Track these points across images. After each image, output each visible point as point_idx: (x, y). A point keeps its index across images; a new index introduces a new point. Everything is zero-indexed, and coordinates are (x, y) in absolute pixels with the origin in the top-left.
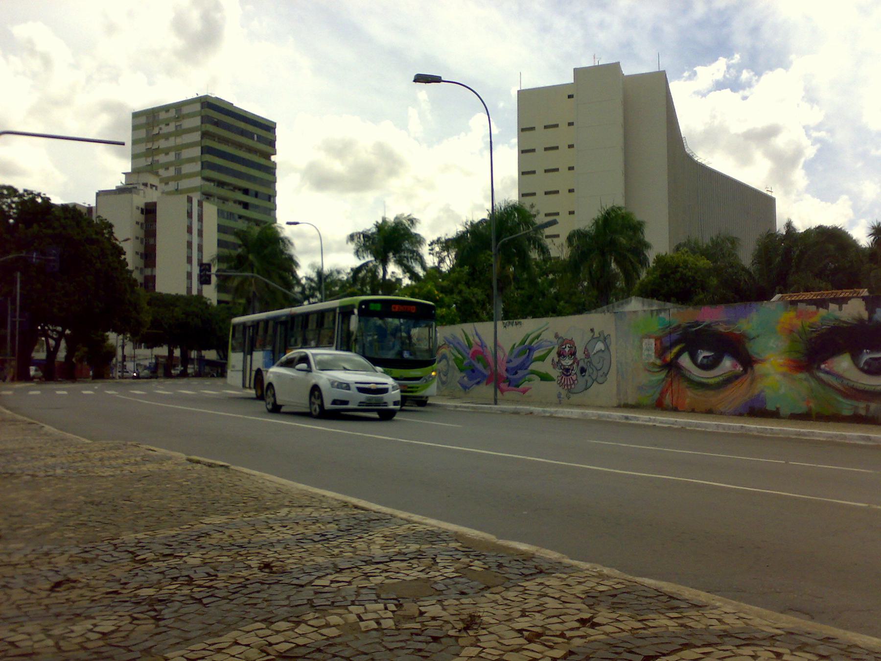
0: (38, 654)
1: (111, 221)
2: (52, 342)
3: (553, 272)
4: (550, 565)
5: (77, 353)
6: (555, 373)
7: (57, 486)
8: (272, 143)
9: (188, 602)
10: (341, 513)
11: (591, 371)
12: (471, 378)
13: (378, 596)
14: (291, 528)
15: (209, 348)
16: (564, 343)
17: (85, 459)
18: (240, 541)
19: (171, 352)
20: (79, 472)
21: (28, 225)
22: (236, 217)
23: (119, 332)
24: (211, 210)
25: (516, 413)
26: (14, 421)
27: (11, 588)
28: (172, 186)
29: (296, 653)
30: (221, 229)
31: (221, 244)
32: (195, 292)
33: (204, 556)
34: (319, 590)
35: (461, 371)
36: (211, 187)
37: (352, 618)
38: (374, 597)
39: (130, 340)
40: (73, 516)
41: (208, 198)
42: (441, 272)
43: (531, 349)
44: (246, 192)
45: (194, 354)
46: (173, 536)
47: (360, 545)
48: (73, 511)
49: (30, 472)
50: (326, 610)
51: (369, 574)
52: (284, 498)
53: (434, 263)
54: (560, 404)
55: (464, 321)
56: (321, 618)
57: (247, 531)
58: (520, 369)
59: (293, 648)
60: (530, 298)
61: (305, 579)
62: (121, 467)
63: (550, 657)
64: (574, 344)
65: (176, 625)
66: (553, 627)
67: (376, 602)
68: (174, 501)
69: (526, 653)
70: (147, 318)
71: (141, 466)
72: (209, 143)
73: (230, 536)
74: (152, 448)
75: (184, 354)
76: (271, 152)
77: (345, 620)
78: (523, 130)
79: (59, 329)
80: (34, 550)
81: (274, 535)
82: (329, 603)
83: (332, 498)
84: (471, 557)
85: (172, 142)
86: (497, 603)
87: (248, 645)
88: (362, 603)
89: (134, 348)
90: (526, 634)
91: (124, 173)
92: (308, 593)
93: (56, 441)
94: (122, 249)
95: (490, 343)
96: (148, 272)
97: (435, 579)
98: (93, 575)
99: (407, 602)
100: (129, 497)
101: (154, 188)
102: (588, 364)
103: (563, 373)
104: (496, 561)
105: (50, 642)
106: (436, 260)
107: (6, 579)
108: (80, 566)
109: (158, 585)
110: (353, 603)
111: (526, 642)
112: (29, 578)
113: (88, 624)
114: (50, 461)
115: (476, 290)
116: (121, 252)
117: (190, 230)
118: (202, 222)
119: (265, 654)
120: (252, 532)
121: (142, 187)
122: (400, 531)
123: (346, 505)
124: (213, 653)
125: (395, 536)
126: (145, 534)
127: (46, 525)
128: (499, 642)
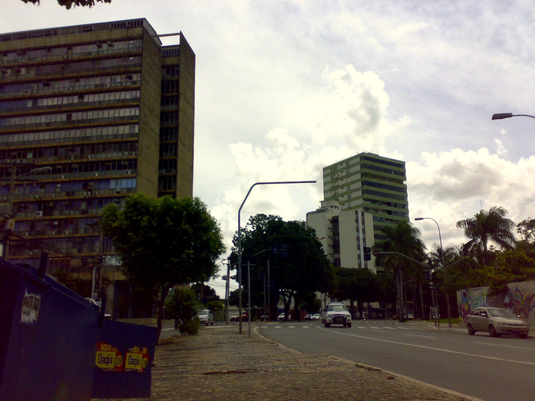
1: (314, 228)
2: (287, 298)
5: (301, 305)
7: (278, 378)
8: (403, 174)
19: (352, 304)
20: (291, 370)
22: (384, 220)
24: (369, 217)
26: (264, 342)
28: (346, 206)
30: (376, 228)
31: (376, 236)
36: (368, 204)
39: (329, 296)
40: (282, 396)
41: (367, 211)
42: (528, 244)
44: (389, 204)
45: (365, 305)
49: (265, 369)
52: (417, 392)
53: (522, 238)
70: (336, 283)
71: (327, 368)
72: (365, 179)
79: (290, 290)
83: (452, 395)
85: (345, 181)
91: (320, 202)
94: (321, 243)
96: (336, 256)
100: (317, 386)
101: (337, 208)
114: (277, 363)
116: (320, 245)
117: (358, 230)
118: (364, 225)
121: (330, 208)
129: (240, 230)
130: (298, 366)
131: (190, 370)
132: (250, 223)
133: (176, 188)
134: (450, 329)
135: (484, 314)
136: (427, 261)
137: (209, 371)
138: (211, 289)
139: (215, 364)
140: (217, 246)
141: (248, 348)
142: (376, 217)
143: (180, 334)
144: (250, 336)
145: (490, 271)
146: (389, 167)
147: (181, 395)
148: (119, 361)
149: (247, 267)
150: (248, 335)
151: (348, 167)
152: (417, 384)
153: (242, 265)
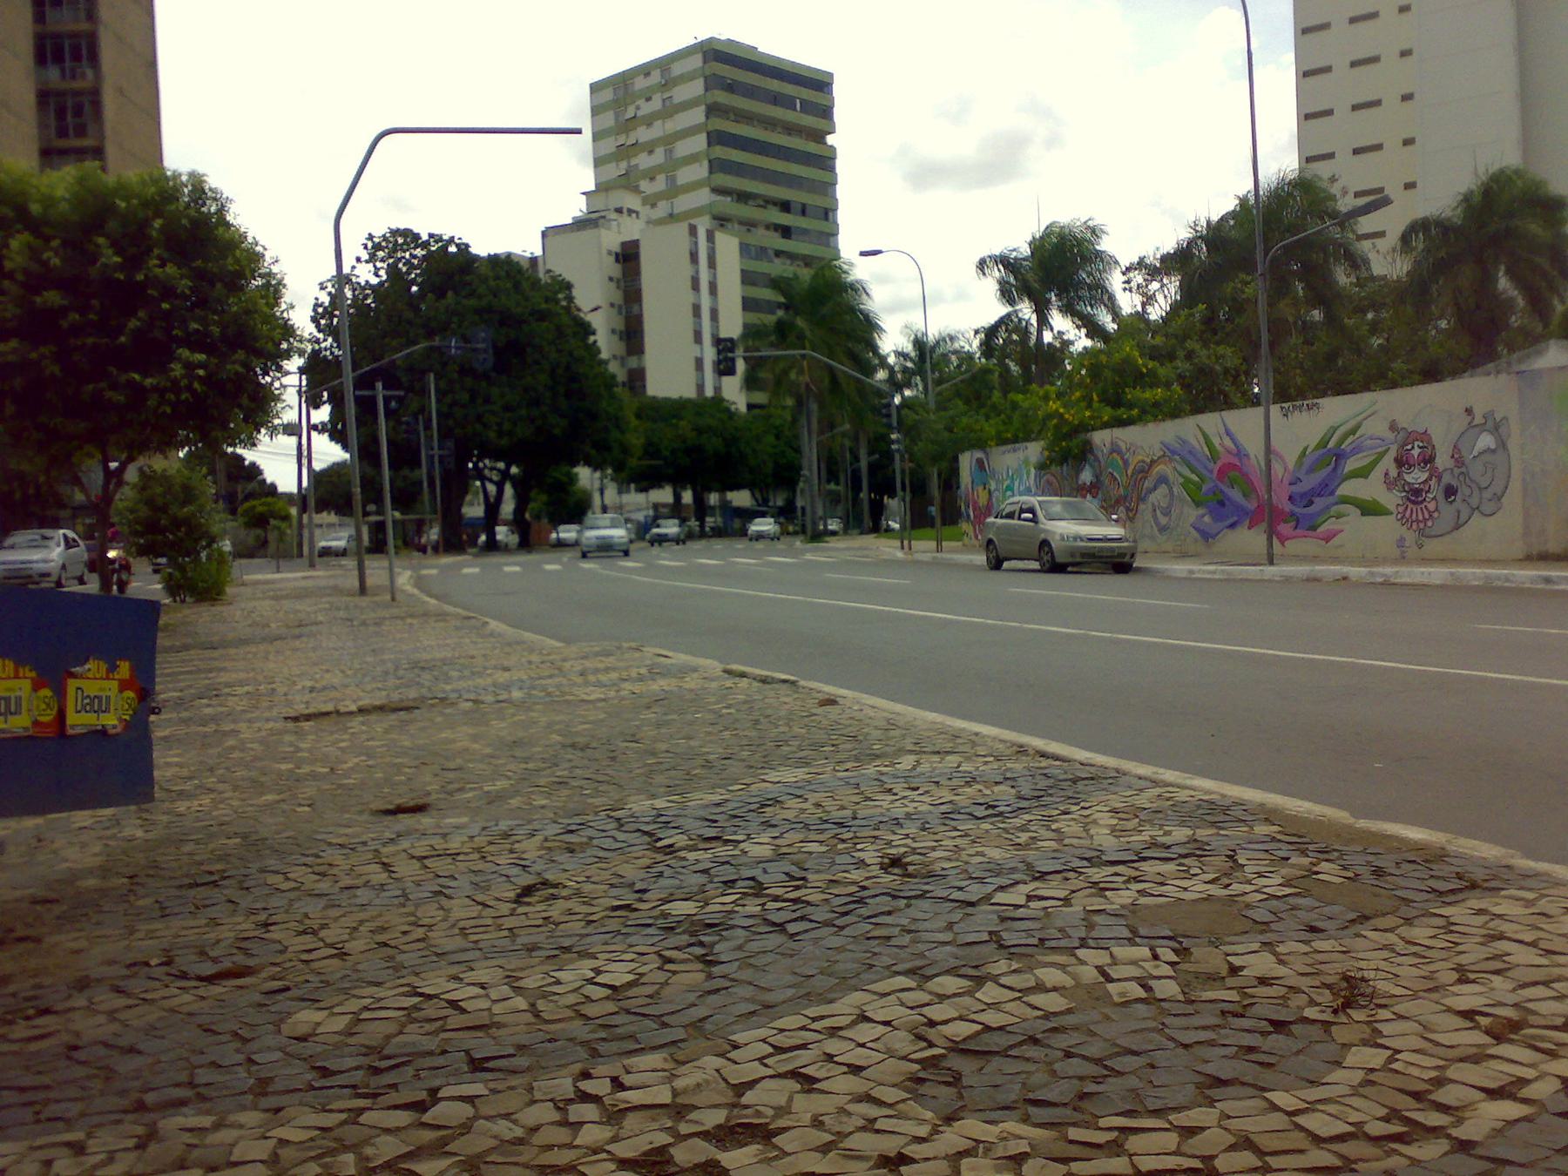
0: (499, 1025)
1: (568, 276)
2: (492, 488)
3: (1375, 306)
4: (1488, 871)
6: (1391, 499)
7: (516, 719)
8: (826, 112)
9: (760, 930)
10: (1018, 766)
11: (1467, 491)
12: (1218, 518)
13: (1134, 932)
14: (927, 792)
15: (737, 487)
16: (1410, 440)
17: (556, 672)
18: (837, 815)
19: (678, 497)
20: (549, 694)
21: (441, 294)
22: (771, 253)
23: (596, 466)
24: (728, 246)
25: (1313, 580)
26: (442, 616)
27: (449, 897)
28: (662, 209)
29: (987, 1044)
30: (748, 278)
31: (748, 304)
32: (709, 392)
33: (778, 842)
34: (1008, 914)
35: (1198, 504)
36: (727, 205)
37: (1089, 974)
38: (1126, 933)
40: (545, 769)
41: (722, 225)
42: (1147, 322)
43: (1340, 456)
44: (785, 207)
45: (713, 499)
46: (718, 805)
47: (1069, 826)
48: (544, 760)
50: (1032, 956)
51: (1102, 885)
52: (904, 737)
54: (1402, 559)
55: (1198, 410)
56: (1025, 972)
57: (848, 796)
58: (1319, 495)
59: (978, 1033)
60: (1331, 357)
61: (975, 891)
62: (614, 685)
63: (1559, 1077)
64: (1430, 440)
65: (746, 974)
66: (1543, 1007)
67: (1131, 942)
68: (710, 742)
69: (1493, 1064)
70: (636, 441)
73: (818, 805)
74: (665, 653)
75: (699, 501)
76: (826, 129)
77: (1074, 977)
78: (1305, 31)
79: (501, 465)
80: (484, 829)
81: (897, 804)
82: (1035, 941)
84: (1310, 854)
85: (657, 130)
86: (1393, 951)
87: (887, 1023)
88: (1103, 943)
89: (620, 492)
90: (1484, 1021)
92: (985, 919)
93: (509, 645)
95: (1254, 448)
96: (633, 362)
97: (1247, 899)
98: (587, 874)
99: (1197, 945)
100: (633, 735)
102: (1462, 478)
103: (1408, 499)
104: (1368, 862)
105: (520, 1003)
106: (1138, 300)
107: (441, 881)
108: (563, 857)
109: (699, 895)
110: (1083, 944)
111: (1488, 1040)
112: (477, 879)
113: (585, 968)
114: (502, 677)
115: (1221, 350)
116: (586, 329)
117: (695, 285)
119: (925, 1044)
120: (856, 799)
121: (614, 216)
122: (1143, 800)
123: (1022, 750)
124: (820, 1037)
125: (1136, 811)
126: (669, 801)
127: (501, 784)
128: (1425, 1038)
129: (342, 279)
130: (565, 681)
131: (239, 708)
132: (365, 256)
133: (101, 136)
134: (939, 555)
135: (1030, 516)
136: (881, 375)
137: (301, 709)
138: (247, 463)
139: (312, 690)
140: (277, 334)
141: (398, 636)
142: (747, 245)
143: (167, 601)
144: (393, 599)
145: (1048, 402)
146: (789, 89)
147: (235, 788)
148: (44, 706)
149: (373, 399)
150: (388, 597)
151: (668, 84)
152: (899, 714)
153: (357, 393)
